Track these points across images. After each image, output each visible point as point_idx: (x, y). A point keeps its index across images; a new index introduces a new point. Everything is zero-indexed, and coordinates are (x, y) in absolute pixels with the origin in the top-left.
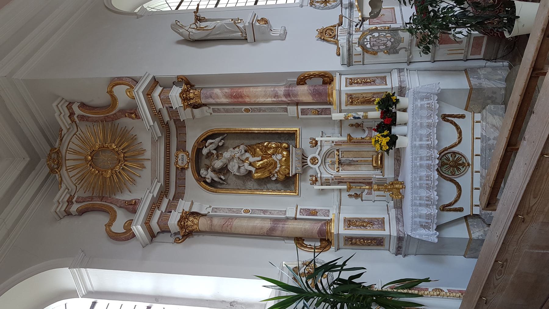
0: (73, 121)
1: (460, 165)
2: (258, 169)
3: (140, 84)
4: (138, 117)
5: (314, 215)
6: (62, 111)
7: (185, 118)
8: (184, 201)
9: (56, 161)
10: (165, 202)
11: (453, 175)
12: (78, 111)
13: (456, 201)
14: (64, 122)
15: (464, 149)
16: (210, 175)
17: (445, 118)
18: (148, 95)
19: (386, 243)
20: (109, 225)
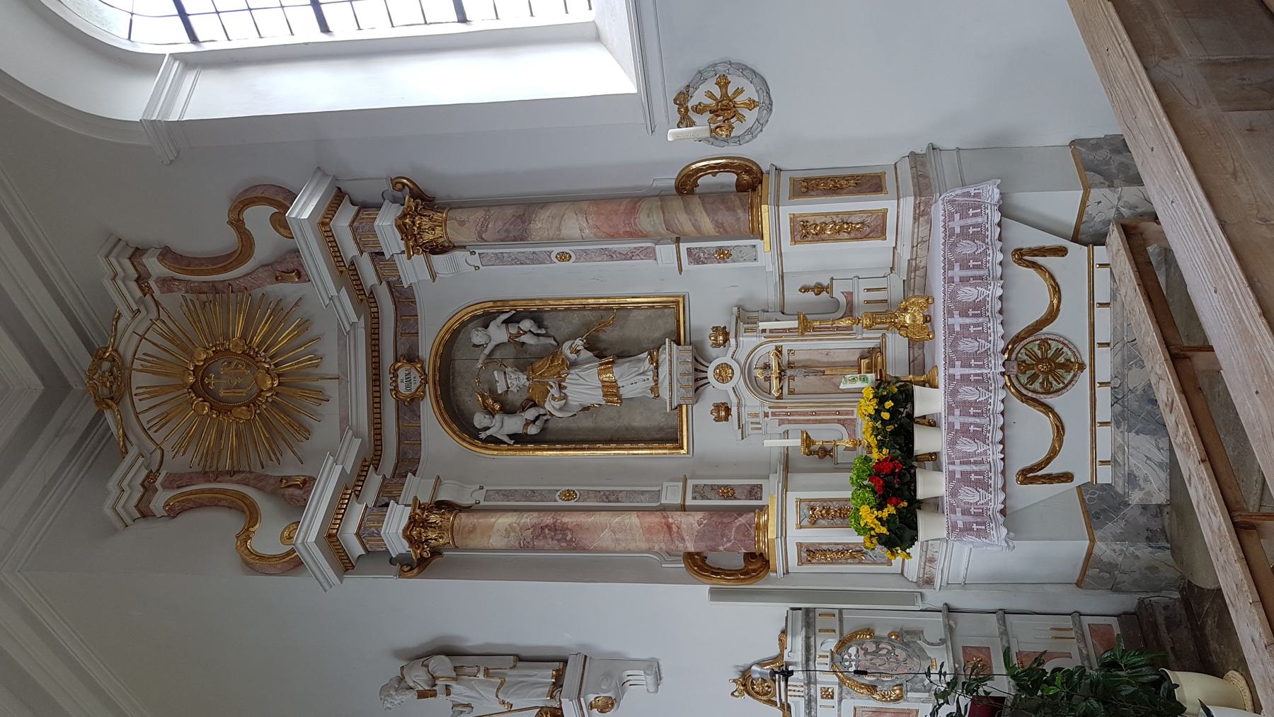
0: (146, 290)
1: (1062, 366)
3: (309, 560)
4: (300, 274)
5: (728, 498)
6: (119, 269)
7: (413, 280)
8: (416, 479)
9: (111, 383)
10: (374, 482)
11: (1048, 392)
12: (154, 266)
13: (1053, 453)
15: (1070, 328)
17: (1023, 256)
18: (323, 224)
19: (889, 182)
20: (245, 535)
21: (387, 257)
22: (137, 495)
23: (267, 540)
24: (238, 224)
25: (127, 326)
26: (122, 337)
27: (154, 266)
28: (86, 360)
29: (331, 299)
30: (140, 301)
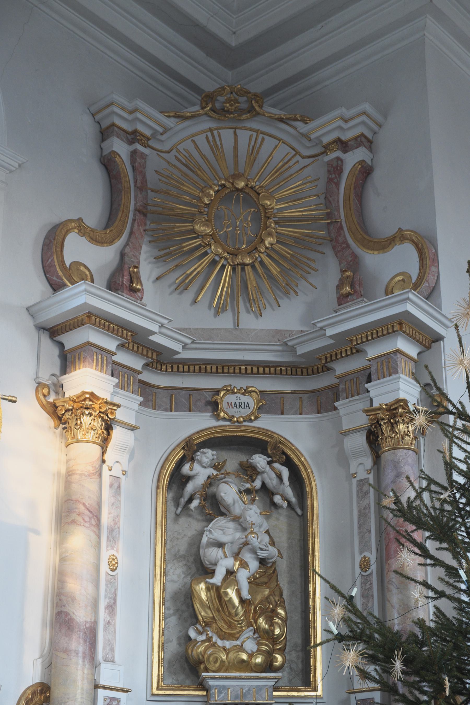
0: (327, 148)
2: (218, 593)
6: (351, 123)
7: (342, 412)
10: (134, 362)
12: (352, 159)
14: (326, 127)
16: (200, 472)
21: (367, 386)
22: (124, 125)
23: (76, 249)
24: (400, 237)
25: (296, 128)
26: (287, 124)
27: (352, 159)
28: (256, 87)
29: (321, 328)
30: (319, 141)
